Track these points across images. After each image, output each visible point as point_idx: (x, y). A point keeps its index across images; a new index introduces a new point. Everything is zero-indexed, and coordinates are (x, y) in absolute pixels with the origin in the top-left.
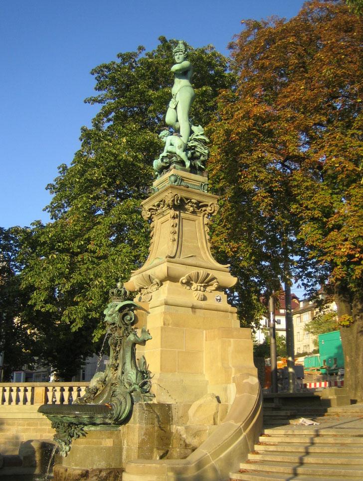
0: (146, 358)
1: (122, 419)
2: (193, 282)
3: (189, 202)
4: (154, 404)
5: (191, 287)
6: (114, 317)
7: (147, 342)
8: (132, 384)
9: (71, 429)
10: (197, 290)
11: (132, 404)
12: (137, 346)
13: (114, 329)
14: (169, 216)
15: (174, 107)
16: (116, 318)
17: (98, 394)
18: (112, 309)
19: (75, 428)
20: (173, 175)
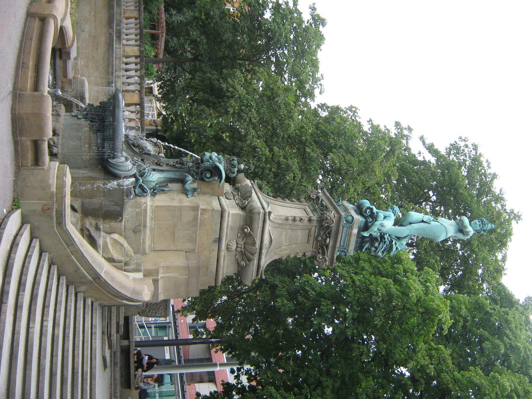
3: (326, 235)
6: (209, 162)
14: (311, 215)
15: (425, 220)
16: (208, 163)
18: (217, 159)
20: (353, 217)
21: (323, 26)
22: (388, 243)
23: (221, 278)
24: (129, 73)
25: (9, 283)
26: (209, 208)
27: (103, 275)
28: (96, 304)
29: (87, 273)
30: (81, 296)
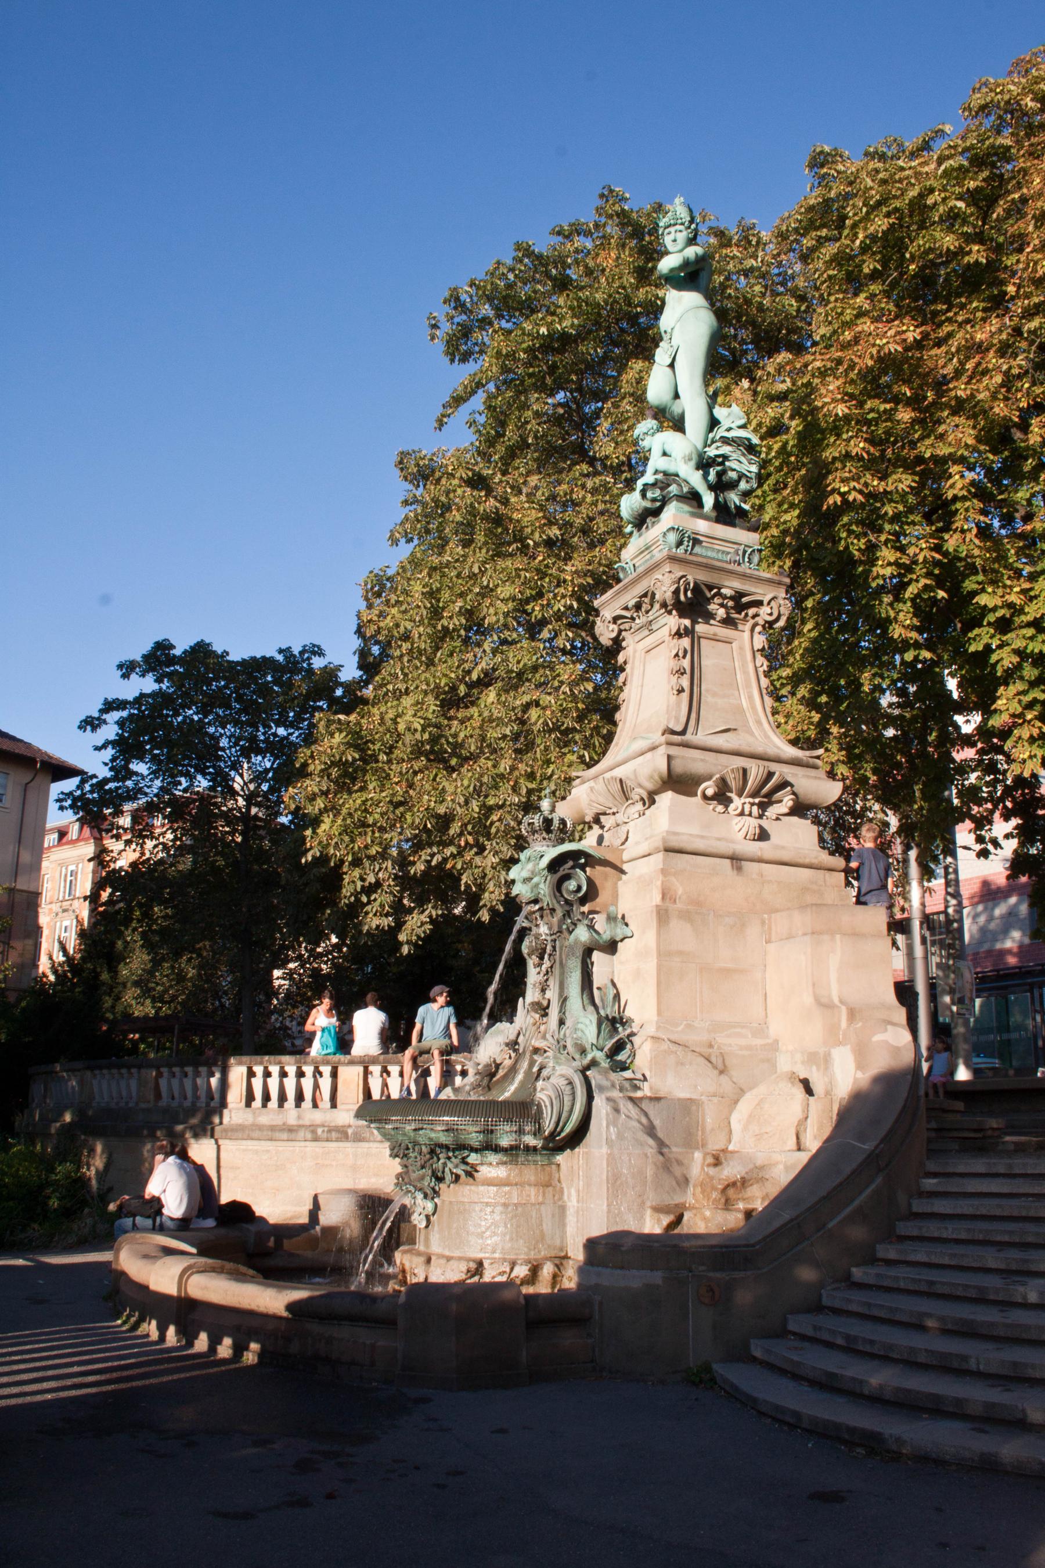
0: (618, 986)
1: (563, 1134)
5: (727, 807)
6: (537, 885)
8: (588, 1047)
9: (439, 1159)
10: (742, 814)
11: (590, 1098)
12: (596, 956)
15: (669, 361)
16: (542, 886)
17: (498, 1077)
21: (173, 647)
22: (726, 450)
23: (824, 857)
24: (291, 1093)
25: (959, 1402)
26: (659, 883)
27: (868, 1146)
28: (931, 1166)
29: (867, 1187)
30: (919, 1206)
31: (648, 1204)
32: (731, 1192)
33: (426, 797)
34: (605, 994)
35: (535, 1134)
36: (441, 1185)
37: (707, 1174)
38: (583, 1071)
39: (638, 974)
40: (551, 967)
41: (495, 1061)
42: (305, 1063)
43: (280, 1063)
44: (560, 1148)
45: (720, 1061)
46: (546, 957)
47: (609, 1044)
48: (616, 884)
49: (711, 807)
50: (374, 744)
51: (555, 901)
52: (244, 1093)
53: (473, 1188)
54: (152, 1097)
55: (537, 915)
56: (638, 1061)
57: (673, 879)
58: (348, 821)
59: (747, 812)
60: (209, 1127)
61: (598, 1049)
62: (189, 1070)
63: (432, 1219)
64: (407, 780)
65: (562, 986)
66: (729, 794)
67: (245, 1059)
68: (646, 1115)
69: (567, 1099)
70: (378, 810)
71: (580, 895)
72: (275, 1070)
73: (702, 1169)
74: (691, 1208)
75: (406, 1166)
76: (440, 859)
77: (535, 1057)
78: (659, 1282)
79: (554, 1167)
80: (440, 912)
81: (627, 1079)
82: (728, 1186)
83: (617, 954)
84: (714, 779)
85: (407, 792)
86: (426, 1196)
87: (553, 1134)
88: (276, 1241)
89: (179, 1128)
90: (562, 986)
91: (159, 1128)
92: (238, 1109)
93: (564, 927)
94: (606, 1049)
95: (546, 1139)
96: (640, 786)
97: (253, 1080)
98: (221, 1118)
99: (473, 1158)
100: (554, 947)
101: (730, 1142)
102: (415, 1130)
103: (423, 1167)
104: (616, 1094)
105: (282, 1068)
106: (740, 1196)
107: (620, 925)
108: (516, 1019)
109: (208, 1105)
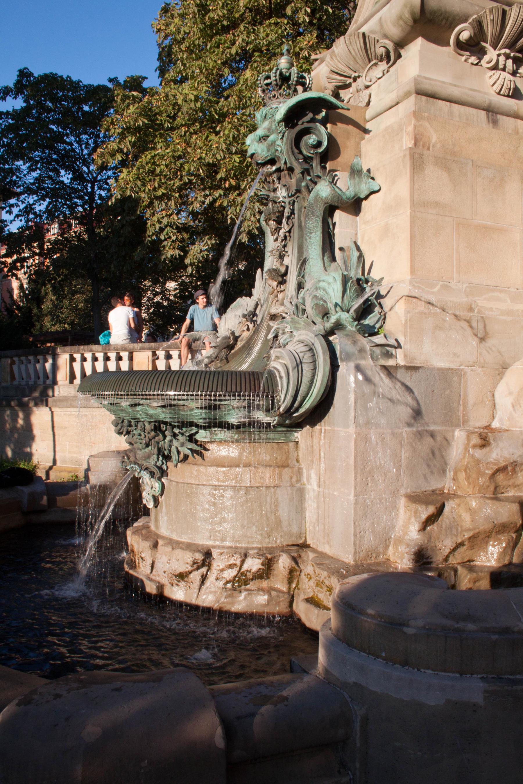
0: (362, 248)
1: (302, 411)
2: (487, 46)
4: (397, 367)
5: (480, 59)
6: (273, 143)
7: (364, 203)
8: (331, 306)
9: (165, 437)
10: (495, 68)
11: (334, 367)
12: (339, 216)
13: (275, 177)
16: (279, 142)
17: (236, 349)
19: (175, 435)
26: (411, 128)
31: (403, 491)
32: (500, 477)
33: (199, 151)
34: (349, 257)
35: (268, 411)
36: (169, 464)
37: (473, 456)
38: (327, 335)
39: (386, 231)
40: (290, 232)
41: (233, 333)
42: (109, 350)
43: (91, 351)
44: (299, 425)
45: (481, 327)
46: (284, 221)
47: (358, 303)
48: (359, 144)
49: (464, 58)
50: (160, 115)
51: (293, 159)
52: (68, 374)
53: (202, 468)
54: (9, 379)
55: (275, 177)
56: (389, 325)
57: (427, 124)
58: (141, 171)
59: (501, 66)
60: (45, 399)
61: (342, 310)
62: (31, 358)
63: (161, 499)
64: (185, 140)
65: (301, 250)
66: (483, 44)
67: (68, 348)
68: (408, 389)
69: (307, 369)
70: (164, 163)
71: (320, 150)
72: (88, 356)
73: (466, 449)
74: (453, 496)
75: (131, 444)
76: (211, 199)
77: (271, 323)
78: (479, 699)
79: (291, 445)
80: (214, 242)
81: (378, 345)
82: (498, 470)
83: (361, 214)
84: (470, 20)
85: (186, 149)
86: (152, 474)
87: (289, 411)
88: (48, 500)
89: (26, 399)
90: (301, 250)
91: (13, 400)
92: (64, 385)
93: (303, 184)
94: (352, 311)
95: (280, 415)
96: (386, 36)
97: (74, 364)
98: (53, 392)
99: (202, 436)
100: (292, 212)
101: (493, 418)
102: (131, 406)
103: (147, 445)
104: (367, 363)
105: (93, 355)
106: (511, 482)
107: (364, 179)
108: (255, 291)
109: (45, 382)
